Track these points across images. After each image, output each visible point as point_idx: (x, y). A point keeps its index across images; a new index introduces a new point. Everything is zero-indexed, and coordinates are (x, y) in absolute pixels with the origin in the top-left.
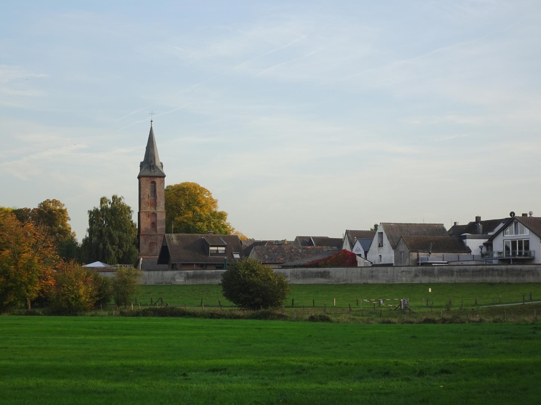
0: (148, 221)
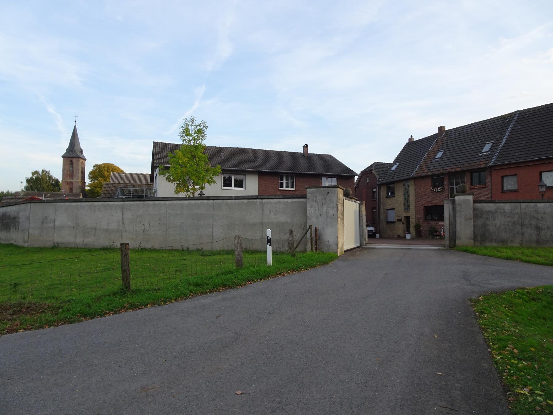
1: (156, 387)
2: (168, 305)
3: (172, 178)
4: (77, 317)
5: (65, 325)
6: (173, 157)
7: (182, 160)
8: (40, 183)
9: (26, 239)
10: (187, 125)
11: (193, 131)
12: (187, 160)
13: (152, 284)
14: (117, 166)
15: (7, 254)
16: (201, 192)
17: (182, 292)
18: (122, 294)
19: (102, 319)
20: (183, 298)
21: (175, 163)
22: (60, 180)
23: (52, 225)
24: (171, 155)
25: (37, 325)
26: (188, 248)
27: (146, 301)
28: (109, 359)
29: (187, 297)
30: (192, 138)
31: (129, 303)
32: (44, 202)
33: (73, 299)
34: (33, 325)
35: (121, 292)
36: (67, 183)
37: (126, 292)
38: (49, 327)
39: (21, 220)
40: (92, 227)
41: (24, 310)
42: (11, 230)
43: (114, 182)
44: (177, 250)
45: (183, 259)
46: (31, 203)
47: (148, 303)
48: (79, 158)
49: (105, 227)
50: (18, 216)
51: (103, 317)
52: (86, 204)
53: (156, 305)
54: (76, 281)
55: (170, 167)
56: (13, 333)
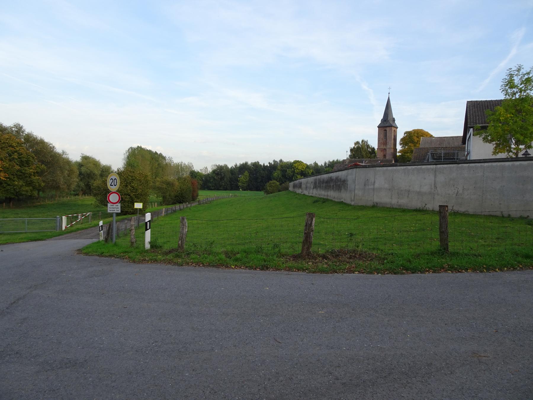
0: (381, 154)
1: (489, 357)
2: (492, 274)
3: (489, 138)
4: (400, 269)
5: (390, 275)
6: (492, 115)
7: (503, 117)
8: (361, 152)
9: (353, 198)
10: (511, 76)
11: (519, 82)
12: (510, 117)
13: (472, 249)
14: (426, 131)
15: (340, 210)
16: (526, 151)
17: (508, 262)
18: (441, 254)
19: (423, 275)
20: (510, 269)
21: (494, 121)
22: (376, 147)
23: (372, 187)
24: (491, 113)
25: (368, 271)
26: (509, 215)
27: (466, 265)
28: (434, 314)
29: (515, 269)
30: (517, 90)
31: (448, 265)
32: (366, 167)
33: (395, 253)
34: (365, 270)
35: (439, 253)
36: (382, 150)
37: (444, 253)
38: (378, 274)
39: (349, 183)
40: (406, 190)
41: (358, 256)
42: (342, 191)
43: (424, 147)
44: (495, 216)
45: (504, 227)
46: (357, 168)
47: (468, 268)
48: (392, 126)
49: (418, 190)
50: (347, 179)
51: (423, 273)
52: (401, 168)
53: (478, 272)
54: (395, 237)
55: (488, 126)
56: (351, 273)
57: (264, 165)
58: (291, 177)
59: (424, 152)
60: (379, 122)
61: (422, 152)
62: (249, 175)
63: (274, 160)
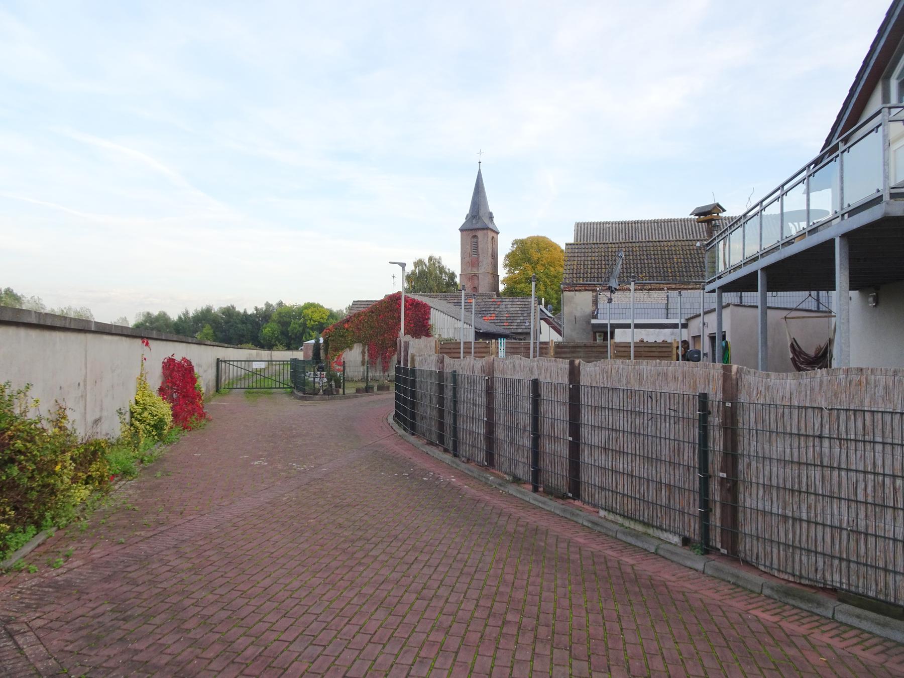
57: (245, 312)
58: (298, 335)
59: (596, 254)
60: (462, 221)
61: (590, 254)
62: (214, 332)
63: (267, 302)
